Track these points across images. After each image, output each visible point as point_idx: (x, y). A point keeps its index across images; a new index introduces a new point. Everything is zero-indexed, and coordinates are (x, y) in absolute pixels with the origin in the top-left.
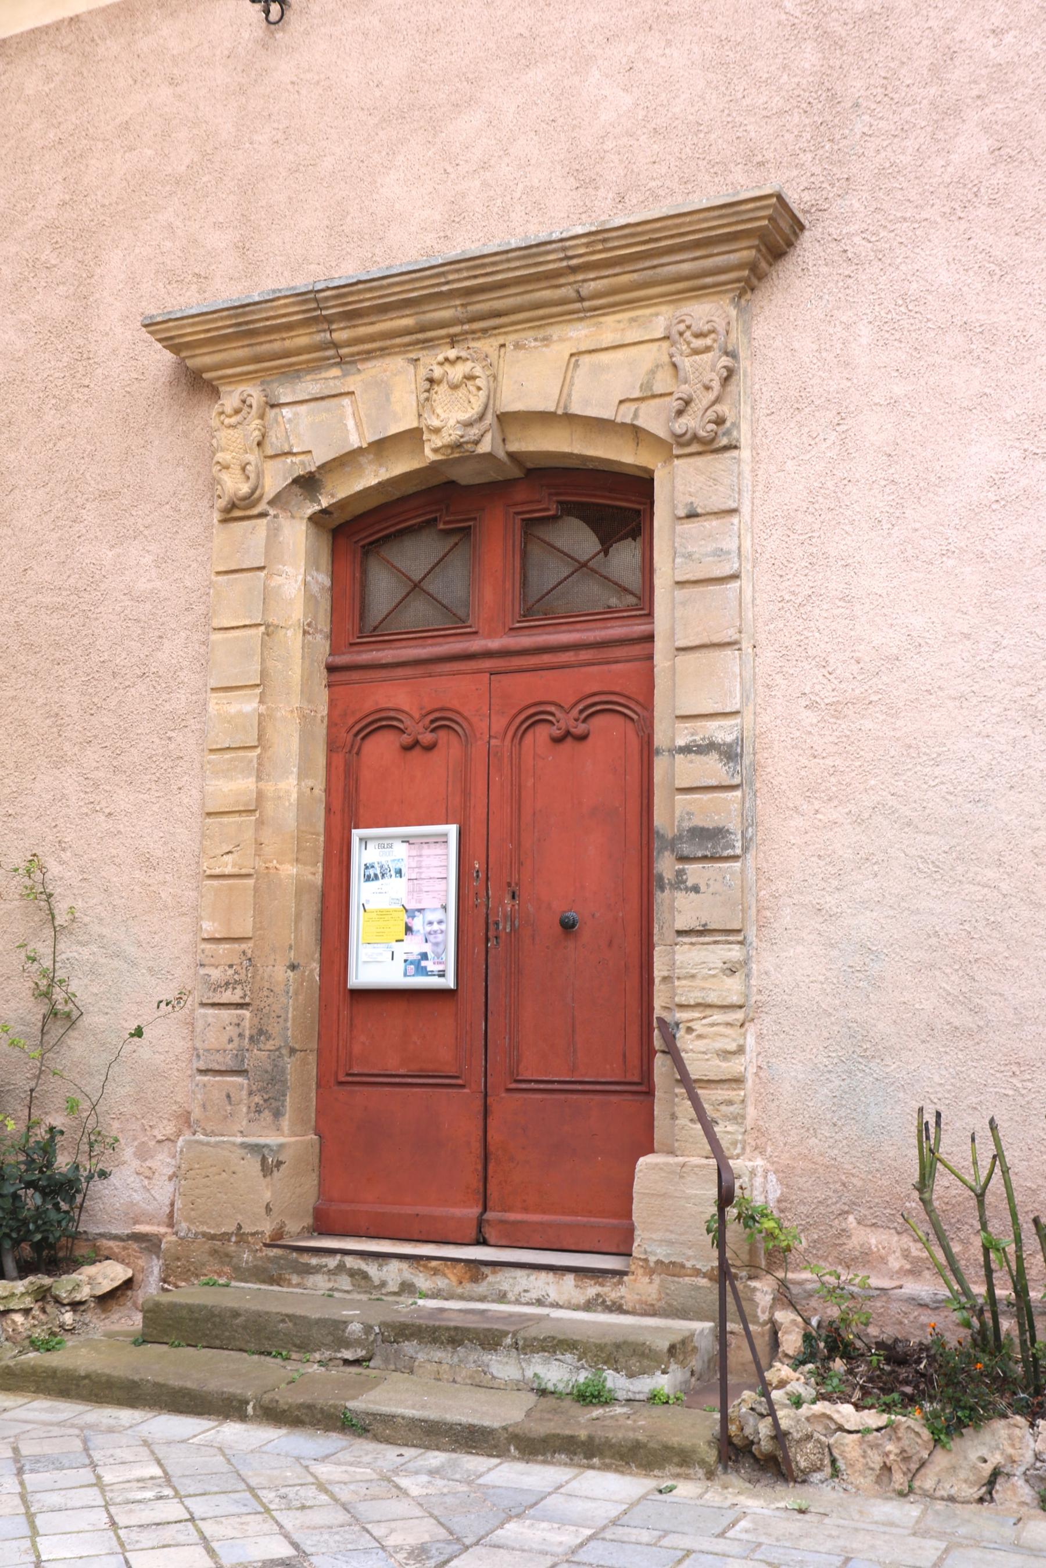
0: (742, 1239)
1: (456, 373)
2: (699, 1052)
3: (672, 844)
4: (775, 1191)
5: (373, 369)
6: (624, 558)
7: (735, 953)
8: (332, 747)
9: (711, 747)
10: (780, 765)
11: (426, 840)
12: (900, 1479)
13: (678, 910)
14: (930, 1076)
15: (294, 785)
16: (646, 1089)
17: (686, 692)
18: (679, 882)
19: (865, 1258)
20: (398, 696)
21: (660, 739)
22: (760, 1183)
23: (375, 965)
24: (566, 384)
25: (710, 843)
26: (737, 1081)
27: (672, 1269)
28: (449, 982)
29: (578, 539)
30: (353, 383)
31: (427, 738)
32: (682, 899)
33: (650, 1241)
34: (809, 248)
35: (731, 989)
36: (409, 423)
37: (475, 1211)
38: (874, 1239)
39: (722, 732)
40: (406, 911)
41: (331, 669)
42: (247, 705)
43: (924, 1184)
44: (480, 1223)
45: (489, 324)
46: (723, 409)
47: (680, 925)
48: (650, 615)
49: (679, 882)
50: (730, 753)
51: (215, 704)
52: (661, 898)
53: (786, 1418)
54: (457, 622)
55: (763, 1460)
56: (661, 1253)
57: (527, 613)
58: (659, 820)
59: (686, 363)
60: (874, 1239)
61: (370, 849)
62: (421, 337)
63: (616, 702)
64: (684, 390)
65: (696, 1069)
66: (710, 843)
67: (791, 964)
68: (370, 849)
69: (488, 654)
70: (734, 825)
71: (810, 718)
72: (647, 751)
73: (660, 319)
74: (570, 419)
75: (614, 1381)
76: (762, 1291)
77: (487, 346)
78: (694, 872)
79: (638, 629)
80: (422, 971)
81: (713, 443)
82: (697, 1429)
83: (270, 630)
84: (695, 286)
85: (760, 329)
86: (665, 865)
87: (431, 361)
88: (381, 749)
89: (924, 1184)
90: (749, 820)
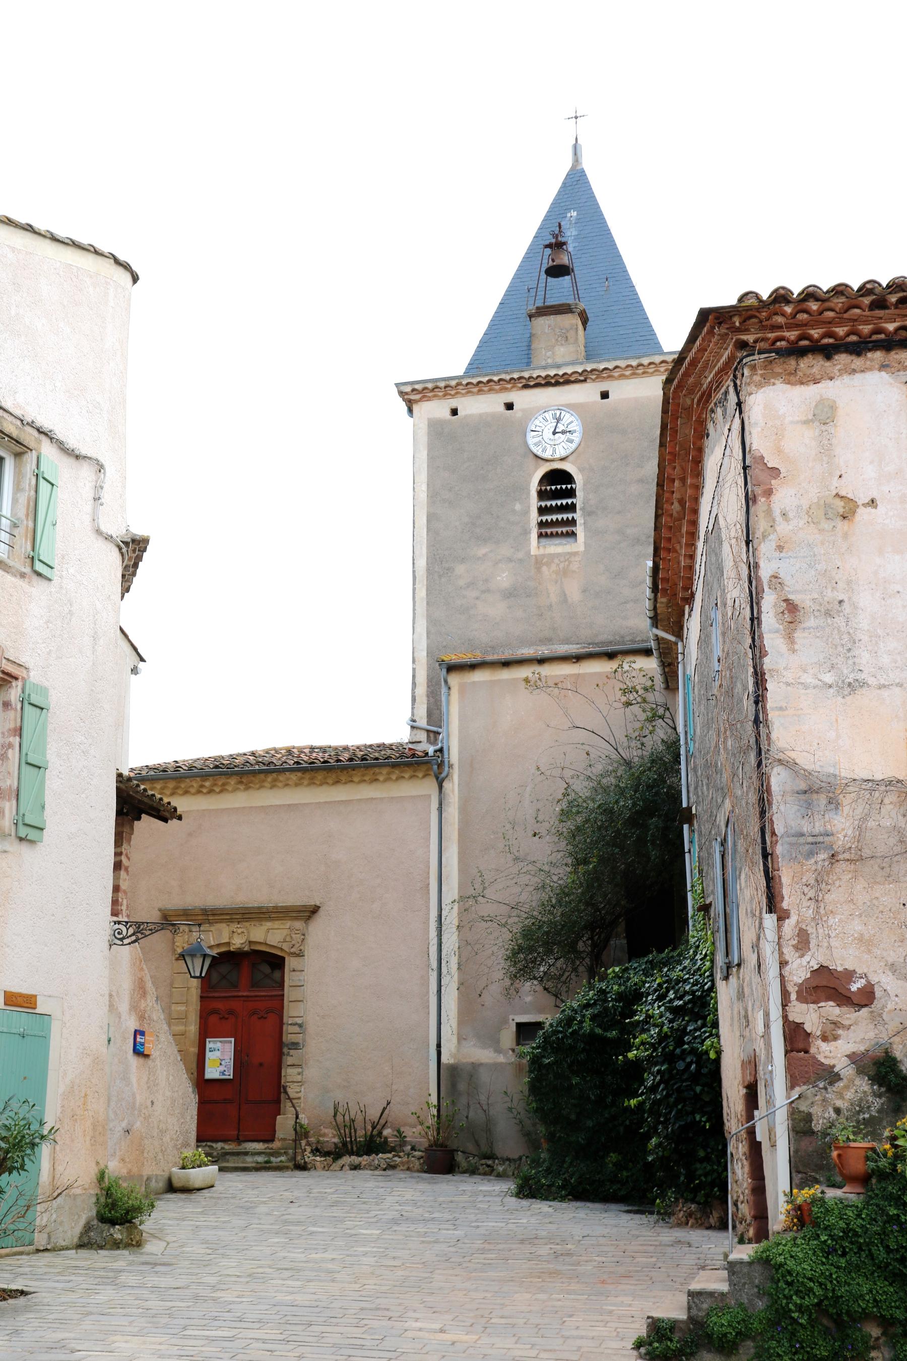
0: (301, 1133)
1: (240, 931)
2: (292, 1092)
3: (287, 1045)
4: (306, 1122)
5: (218, 926)
6: (277, 975)
7: (300, 1070)
8: (201, 1017)
9: (296, 1024)
10: (311, 1029)
11: (226, 1042)
12: (327, 1168)
13: (289, 1060)
14: (339, 1096)
15: (193, 1028)
16: (278, 1102)
17: (291, 1012)
18: (288, 1054)
19: (325, 1135)
20: (219, 1005)
21: (285, 1020)
22: (304, 1119)
23: (212, 1072)
24: (266, 936)
25: (295, 1046)
26: (299, 1098)
27: (284, 1139)
28: (231, 1077)
29: (266, 969)
30: (212, 928)
31: (227, 1016)
32: (289, 1058)
33: (279, 1134)
34: (321, 912)
35: (299, 1078)
36: (226, 940)
37: (236, 1133)
38: (326, 1131)
39: (299, 1021)
40: (220, 1059)
41: (201, 997)
42: (183, 1008)
43: (335, 1115)
44: (238, 1135)
45: (248, 920)
46: (302, 948)
47: (289, 1063)
48: (283, 990)
49: (288, 1054)
50: (300, 1026)
51: (174, 1007)
52: (284, 1057)
53: (307, 1159)
54: (235, 986)
55: (303, 1167)
56: (282, 1136)
57: (253, 986)
58: (284, 1039)
59: (294, 936)
60: (326, 1131)
61: (210, 1044)
62: (231, 921)
63: (275, 1008)
64: (293, 942)
65: (292, 1096)
66: (295, 1046)
67: (312, 1072)
68: (210, 1044)
69: (243, 996)
70: (301, 1042)
71: (318, 1018)
72: (281, 1023)
73: (288, 924)
74: (266, 944)
75: (273, 1159)
76: (303, 1142)
77: (247, 924)
78: (292, 1052)
79: (281, 993)
80: (224, 1074)
81: (300, 955)
82: (291, 1164)
83: (189, 988)
84: (296, 918)
85: (310, 929)
86: (285, 1050)
87: (234, 926)
88: (213, 1019)
89: (335, 1115)
90: (304, 1040)
